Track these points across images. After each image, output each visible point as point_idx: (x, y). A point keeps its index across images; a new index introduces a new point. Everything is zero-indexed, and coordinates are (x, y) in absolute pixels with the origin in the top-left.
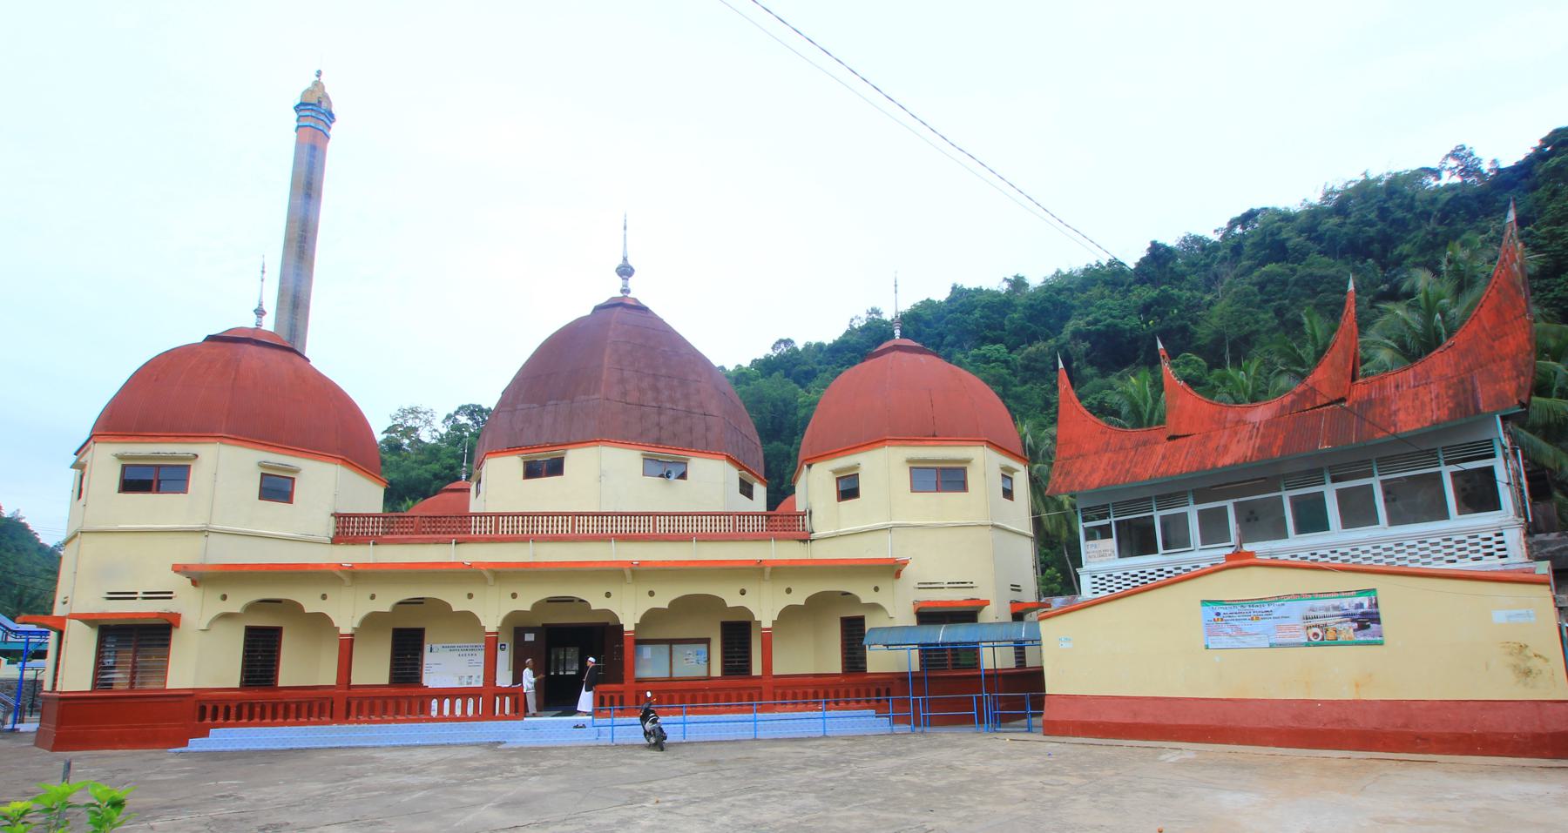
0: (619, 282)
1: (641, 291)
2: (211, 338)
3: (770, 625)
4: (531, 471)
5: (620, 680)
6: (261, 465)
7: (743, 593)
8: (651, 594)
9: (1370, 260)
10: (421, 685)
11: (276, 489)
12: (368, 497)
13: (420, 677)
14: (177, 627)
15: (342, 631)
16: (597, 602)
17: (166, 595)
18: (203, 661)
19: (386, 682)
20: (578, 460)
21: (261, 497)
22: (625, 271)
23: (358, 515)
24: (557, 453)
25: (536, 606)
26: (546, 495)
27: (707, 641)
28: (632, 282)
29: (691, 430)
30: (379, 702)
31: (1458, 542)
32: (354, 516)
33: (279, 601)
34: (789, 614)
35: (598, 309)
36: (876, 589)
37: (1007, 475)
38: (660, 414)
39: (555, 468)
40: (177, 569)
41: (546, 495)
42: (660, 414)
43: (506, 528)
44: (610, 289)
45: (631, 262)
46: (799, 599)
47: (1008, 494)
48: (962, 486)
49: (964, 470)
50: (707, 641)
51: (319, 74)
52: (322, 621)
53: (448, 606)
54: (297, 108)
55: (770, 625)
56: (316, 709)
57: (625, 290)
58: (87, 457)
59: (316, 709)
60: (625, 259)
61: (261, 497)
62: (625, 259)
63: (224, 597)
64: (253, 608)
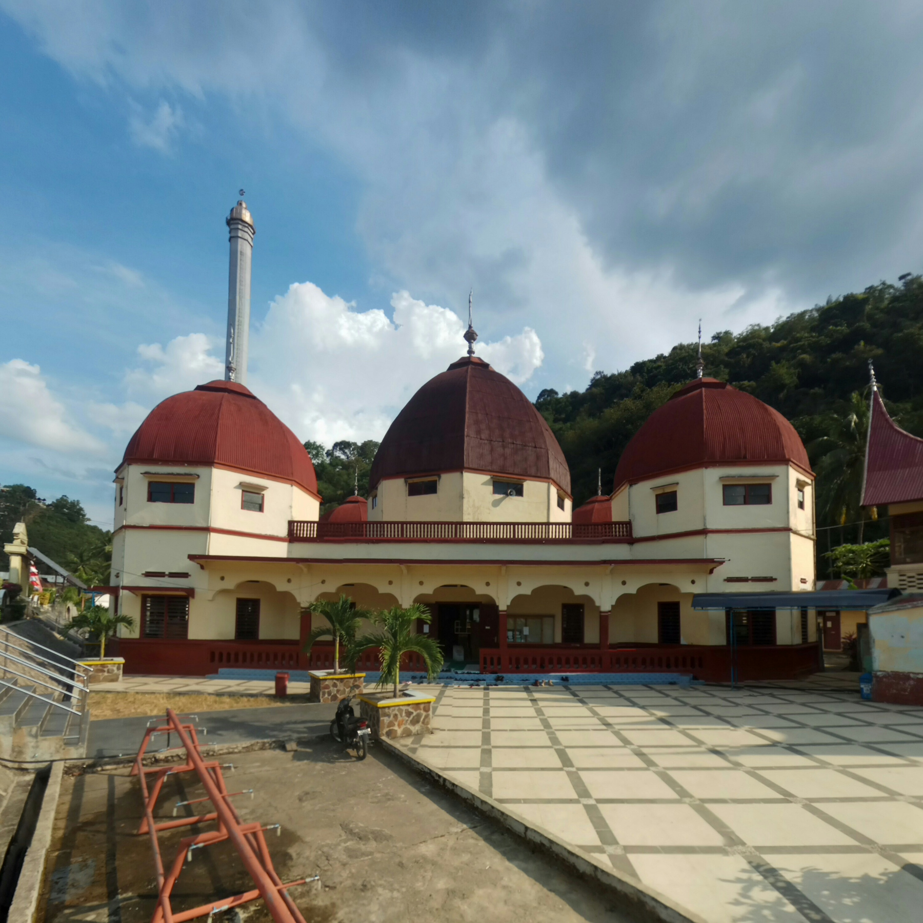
1: (481, 351)
2: (199, 388)
4: (414, 490)
5: (497, 646)
7: (289, 581)
8: (421, 583)
11: (253, 500)
12: (307, 508)
14: (193, 597)
15: (302, 605)
16: (480, 589)
17: (185, 575)
18: (209, 622)
21: (242, 508)
23: (307, 522)
25: (436, 591)
26: (423, 509)
27: (553, 616)
29: (526, 459)
31: (910, 577)
32: (304, 522)
33: (352, 585)
35: (453, 367)
36: (289, 581)
37: (13, 825)
40: (191, 557)
41: (423, 509)
42: (504, 447)
43: (409, 532)
46: (632, 588)
52: (287, 597)
53: (374, 590)
57: (470, 352)
58: (124, 474)
60: (470, 327)
62: (470, 327)
63: (222, 578)
64: (241, 586)
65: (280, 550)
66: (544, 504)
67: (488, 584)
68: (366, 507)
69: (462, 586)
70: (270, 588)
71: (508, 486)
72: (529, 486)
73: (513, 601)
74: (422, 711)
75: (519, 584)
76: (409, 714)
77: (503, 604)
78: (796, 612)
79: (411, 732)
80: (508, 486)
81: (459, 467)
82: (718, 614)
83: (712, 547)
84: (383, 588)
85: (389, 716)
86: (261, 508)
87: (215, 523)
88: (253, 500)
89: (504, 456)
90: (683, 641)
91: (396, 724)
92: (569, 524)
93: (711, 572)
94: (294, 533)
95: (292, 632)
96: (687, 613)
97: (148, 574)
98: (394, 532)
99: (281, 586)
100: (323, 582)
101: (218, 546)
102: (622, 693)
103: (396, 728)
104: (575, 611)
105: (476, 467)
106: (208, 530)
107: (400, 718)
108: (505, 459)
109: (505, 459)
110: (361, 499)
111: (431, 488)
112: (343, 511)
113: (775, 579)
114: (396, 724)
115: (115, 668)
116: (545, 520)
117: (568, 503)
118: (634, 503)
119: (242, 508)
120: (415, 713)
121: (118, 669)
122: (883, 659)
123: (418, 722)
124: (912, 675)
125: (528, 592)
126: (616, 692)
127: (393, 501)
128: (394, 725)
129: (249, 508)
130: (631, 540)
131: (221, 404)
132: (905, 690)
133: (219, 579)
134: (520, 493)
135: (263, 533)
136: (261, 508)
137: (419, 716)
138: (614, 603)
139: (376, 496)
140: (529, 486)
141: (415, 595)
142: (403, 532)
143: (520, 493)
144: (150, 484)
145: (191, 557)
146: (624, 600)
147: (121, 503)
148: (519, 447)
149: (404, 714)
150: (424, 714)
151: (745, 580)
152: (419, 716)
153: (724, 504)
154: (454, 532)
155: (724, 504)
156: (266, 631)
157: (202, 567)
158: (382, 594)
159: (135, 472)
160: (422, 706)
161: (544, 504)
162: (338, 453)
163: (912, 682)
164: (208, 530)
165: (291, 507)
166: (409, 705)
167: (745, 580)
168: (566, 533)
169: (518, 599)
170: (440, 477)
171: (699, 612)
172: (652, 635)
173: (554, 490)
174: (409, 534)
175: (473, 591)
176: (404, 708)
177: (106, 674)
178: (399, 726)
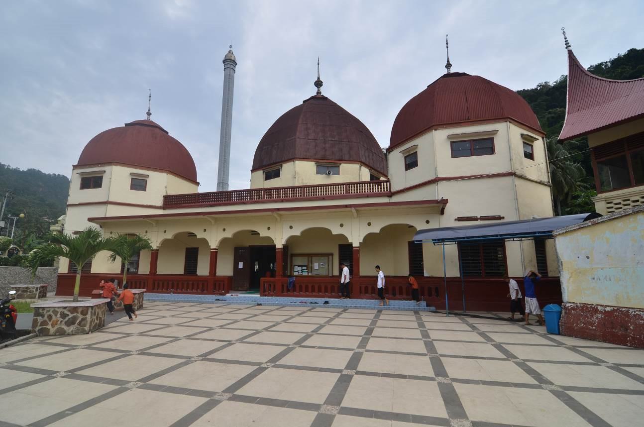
0: (316, 89)
3: (358, 245)
6: (131, 174)
7: (269, 228)
8: (291, 227)
9: (535, 313)
10: (197, 275)
11: (139, 184)
13: (196, 271)
19: (182, 273)
20: (287, 169)
21: (132, 188)
22: (318, 84)
24: (276, 168)
27: (332, 255)
28: (322, 89)
30: (161, 283)
34: (369, 239)
36: (269, 228)
37: (528, 142)
38: (325, 143)
39: (277, 174)
40: (90, 220)
42: (325, 143)
44: (312, 92)
45: (321, 79)
46: (376, 229)
47: (530, 156)
48: (492, 151)
49: (492, 140)
50: (332, 255)
51: (231, 46)
53: (330, 231)
54: (224, 62)
55: (358, 245)
56: (185, 286)
59: (185, 286)
60: (319, 78)
61: (132, 188)
62: (319, 78)
64: (236, 235)
71: (327, 164)
74: (79, 315)
76: (64, 316)
77: (279, 244)
78: (528, 245)
79: (65, 332)
82: (452, 249)
84: (336, 230)
85: (43, 316)
88: (139, 184)
91: (50, 323)
93: (442, 213)
96: (429, 251)
97: (460, 219)
102: (491, 335)
103: (49, 327)
105: (304, 157)
107: (54, 318)
108: (326, 151)
109: (326, 151)
113: (456, 220)
114: (50, 323)
115: (34, 290)
120: (71, 316)
121: (37, 290)
122: (574, 292)
123: (73, 323)
124: (599, 308)
125: (377, 230)
126: (482, 334)
128: (47, 324)
132: (592, 324)
133: (222, 230)
135: (145, 204)
137: (75, 318)
138: (361, 241)
144: (452, 143)
145: (90, 220)
149: (59, 315)
150: (81, 317)
151: (475, 219)
152: (75, 318)
160: (80, 310)
163: (600, 316)
166: (65, 308)
167: (475, 219)
169: (292, 240)
170: (281, 166)
171: (438, 248)
176: (61, 310)
177: (29, 293)
178: (53, 326)
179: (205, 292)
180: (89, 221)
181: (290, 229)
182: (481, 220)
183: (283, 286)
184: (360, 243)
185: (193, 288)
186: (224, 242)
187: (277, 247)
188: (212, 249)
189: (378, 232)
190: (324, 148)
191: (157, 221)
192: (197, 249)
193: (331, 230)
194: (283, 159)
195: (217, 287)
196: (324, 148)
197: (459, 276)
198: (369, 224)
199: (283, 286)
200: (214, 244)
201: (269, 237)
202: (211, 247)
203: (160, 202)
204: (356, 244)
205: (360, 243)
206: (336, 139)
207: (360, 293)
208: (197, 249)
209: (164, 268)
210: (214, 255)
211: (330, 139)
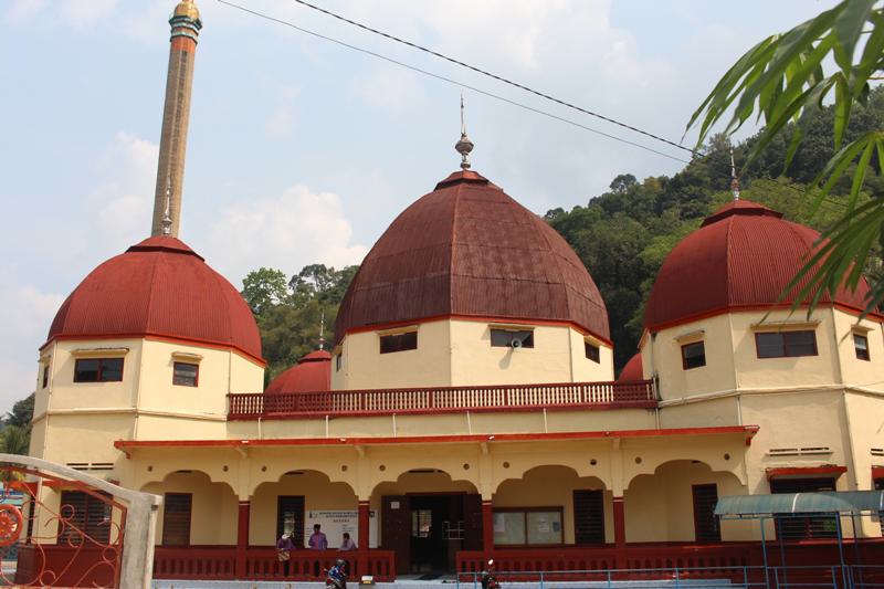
1: (480, 164)
4: (388, 346)
7: (344, 468)
8: (382, 468)
11: (186, 372)
12: (250, 377)
15: (241, 499)
16: (457, 474)
21: (174, 383)
25: (401, 477)
26: (400, 371)
27: (560, 509)
33: (300, 473)
36: (226, 469)
40: (118, 445)
42: (504, 285)
46: (649, 467)
52: (224, 490)
53: (325, 477)
64: (170, 477)
65: (220, 432)
66: (563, 357)
67: (466, 467)
68: (330, 365)
69: (440, 471)
70: (203, 478)
71: (514, 336)
72: (541, 333)
73: (500, 488)
75: (638, 461)
80: (514, 336)
81: (444, 314)
83: (746, 417)
84: (335, 476)
86: (195, 382)
87: (142, 408)
88: (186, 372)
89: (504, 297)
90: (725, 537)
92: (609, 384)
93: (748, 443)
94: (240, 408)
95: (229, 537)
98: (353, 404)
99: (217, 476)
100: (264, 469)
101: (147, 431)
104: (590, 500)
106: (135, 414)
110: (326, 354)
111: (409, 343)
112: (300, 376)
116: (569, 381)
117: (606, 353)
118: (660, 353)
119: (174, 383)
125: (275, 479)
127: (362, 362)
129: (179, 384)
130: (653, 406)
131: (154, 267)
133: (146, 468)
134: (528, 343)
136: (195, 382)
138: (495, 492)
139: (340, 355)
140: (541, 333)
141: (375, 483)
142: (369, 404)
143: (528, 343)
146: (639, 483)
147: (45, 385)
148: (524, 283)
153: (759, 357)
154: (437, 400)
155: (759, 357)
156: (198, 537)
157: (128, 456)
158: (334, 483)
159: (63, 354)
161: (563, 357)
162: (309, 280)
164: (135, 414)
165: (462, 107)
168: (607, 395)
169: (507, 485)
172: (688, 532)
173: (578, 340)
174: (371, 406)
175: (707, 468)
179: (177, 574)
180: (117, 447)
181: (464, 470)
182: (26, 466)
183: (248, 563)
184: (624, 491)
185: (217, 571)
186: (264, 489)
187: (484, 498)
188: (361, 502)
189: (395, 480)
190: (504, 295)
191: (366, 447)
192: (302, 498)
193: (577, 469)
194: (423, 314)
195: (168, 569)
196: (504, 295)
197: (774, 538)
198: (506, 465)
199: (248, 563)
200: (244, 493)
201: (227, 484)
202: (360, 499)
203: (221, 409)
204: (486, 495)
205: (624, 491)
206: (523, 278)
207: (248, 571)
208: (302, 498)
209: (640, 530)
210: (244, 511)
211: (513, 276)
